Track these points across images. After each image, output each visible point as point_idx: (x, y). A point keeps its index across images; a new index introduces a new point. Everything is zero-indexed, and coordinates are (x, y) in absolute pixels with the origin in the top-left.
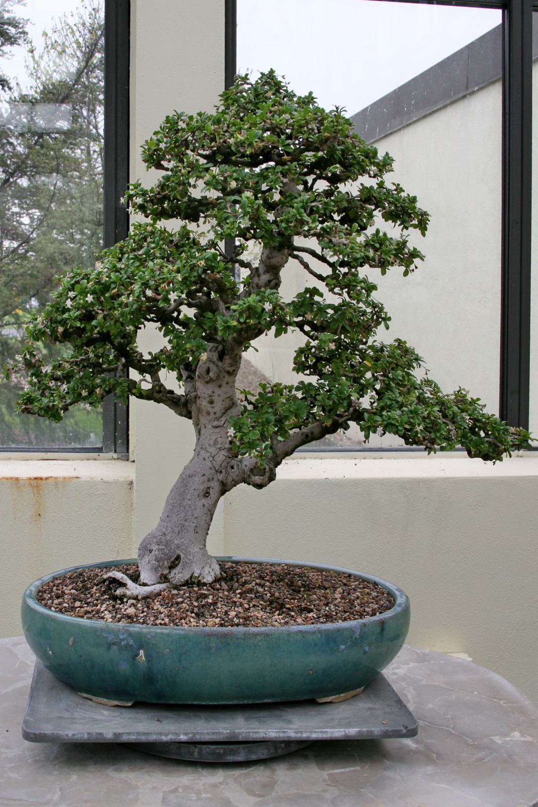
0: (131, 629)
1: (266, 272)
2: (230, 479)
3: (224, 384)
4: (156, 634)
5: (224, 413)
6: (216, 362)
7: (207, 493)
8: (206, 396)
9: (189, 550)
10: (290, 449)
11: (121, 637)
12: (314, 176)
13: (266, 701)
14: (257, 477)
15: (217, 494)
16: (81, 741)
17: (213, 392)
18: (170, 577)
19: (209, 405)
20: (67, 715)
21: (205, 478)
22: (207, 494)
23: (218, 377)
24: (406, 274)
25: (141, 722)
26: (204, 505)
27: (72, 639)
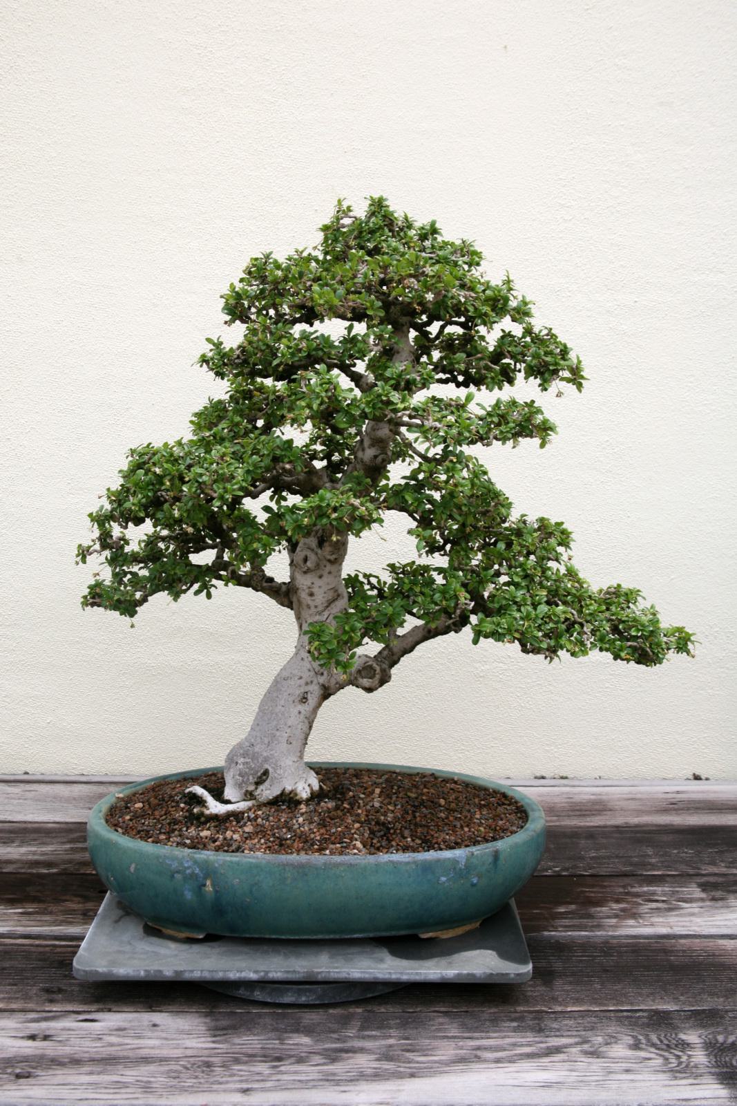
0: (197, 856)
1: (372, 445)
2: (333, 682)
3: (325, 574)
4: (225, 861)
5: (327, 607)
6: (315, 549)
7: (304, 698)
8: (305, 587)
9: (279, 763)
10: (409, 646)
11: (186, 865)
12: (441, 323)
13: (355, 936)
14: (365, 680)
15: (316, 699)
16: (124, 979)
17: (313, 583)
18: (256, 794)
19: (309, 598)
20: (128, 948)
21: (302, 681)
22: (304, 699)
23: (318, 566)
24: (542, 446)
25: (209, 958)
26: (300, 713)
27: (133, 866)
